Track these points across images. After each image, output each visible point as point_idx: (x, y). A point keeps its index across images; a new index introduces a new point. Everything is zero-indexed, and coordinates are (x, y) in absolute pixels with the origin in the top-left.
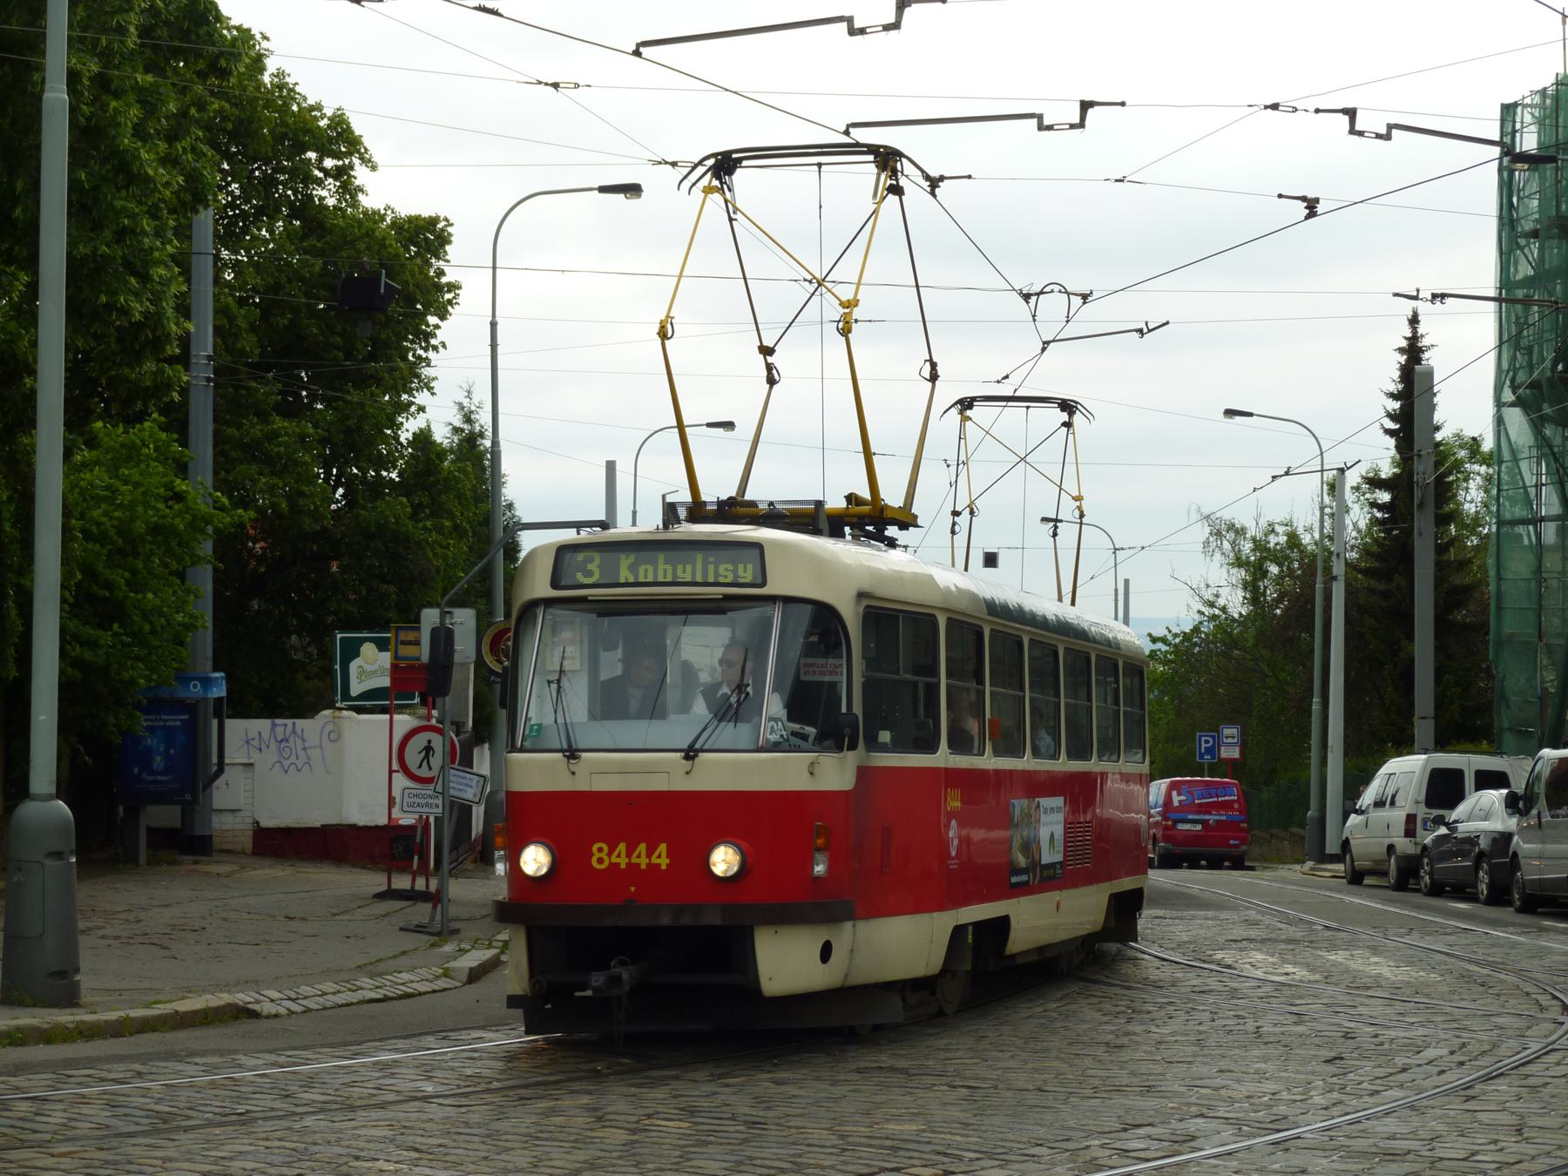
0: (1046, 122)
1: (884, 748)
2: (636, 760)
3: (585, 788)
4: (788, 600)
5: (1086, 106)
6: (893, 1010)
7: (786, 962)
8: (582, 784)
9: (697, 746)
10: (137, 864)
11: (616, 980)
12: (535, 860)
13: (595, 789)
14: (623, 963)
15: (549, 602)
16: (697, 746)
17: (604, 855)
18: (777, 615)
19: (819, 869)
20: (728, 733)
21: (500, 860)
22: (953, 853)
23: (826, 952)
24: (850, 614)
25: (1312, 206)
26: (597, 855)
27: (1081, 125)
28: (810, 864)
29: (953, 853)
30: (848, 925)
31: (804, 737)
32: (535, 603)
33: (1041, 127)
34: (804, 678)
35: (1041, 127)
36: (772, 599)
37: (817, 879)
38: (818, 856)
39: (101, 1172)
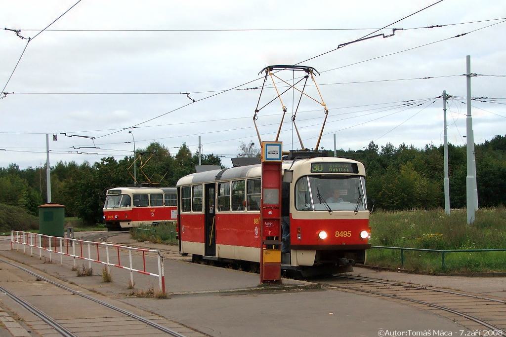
0: (382, 36)
5: (394, 30)
7: (123, 225)
15: (310, 176)
23: (129, 224)
27: (394, 35)
33: (384, 37)
35: (384, 37)
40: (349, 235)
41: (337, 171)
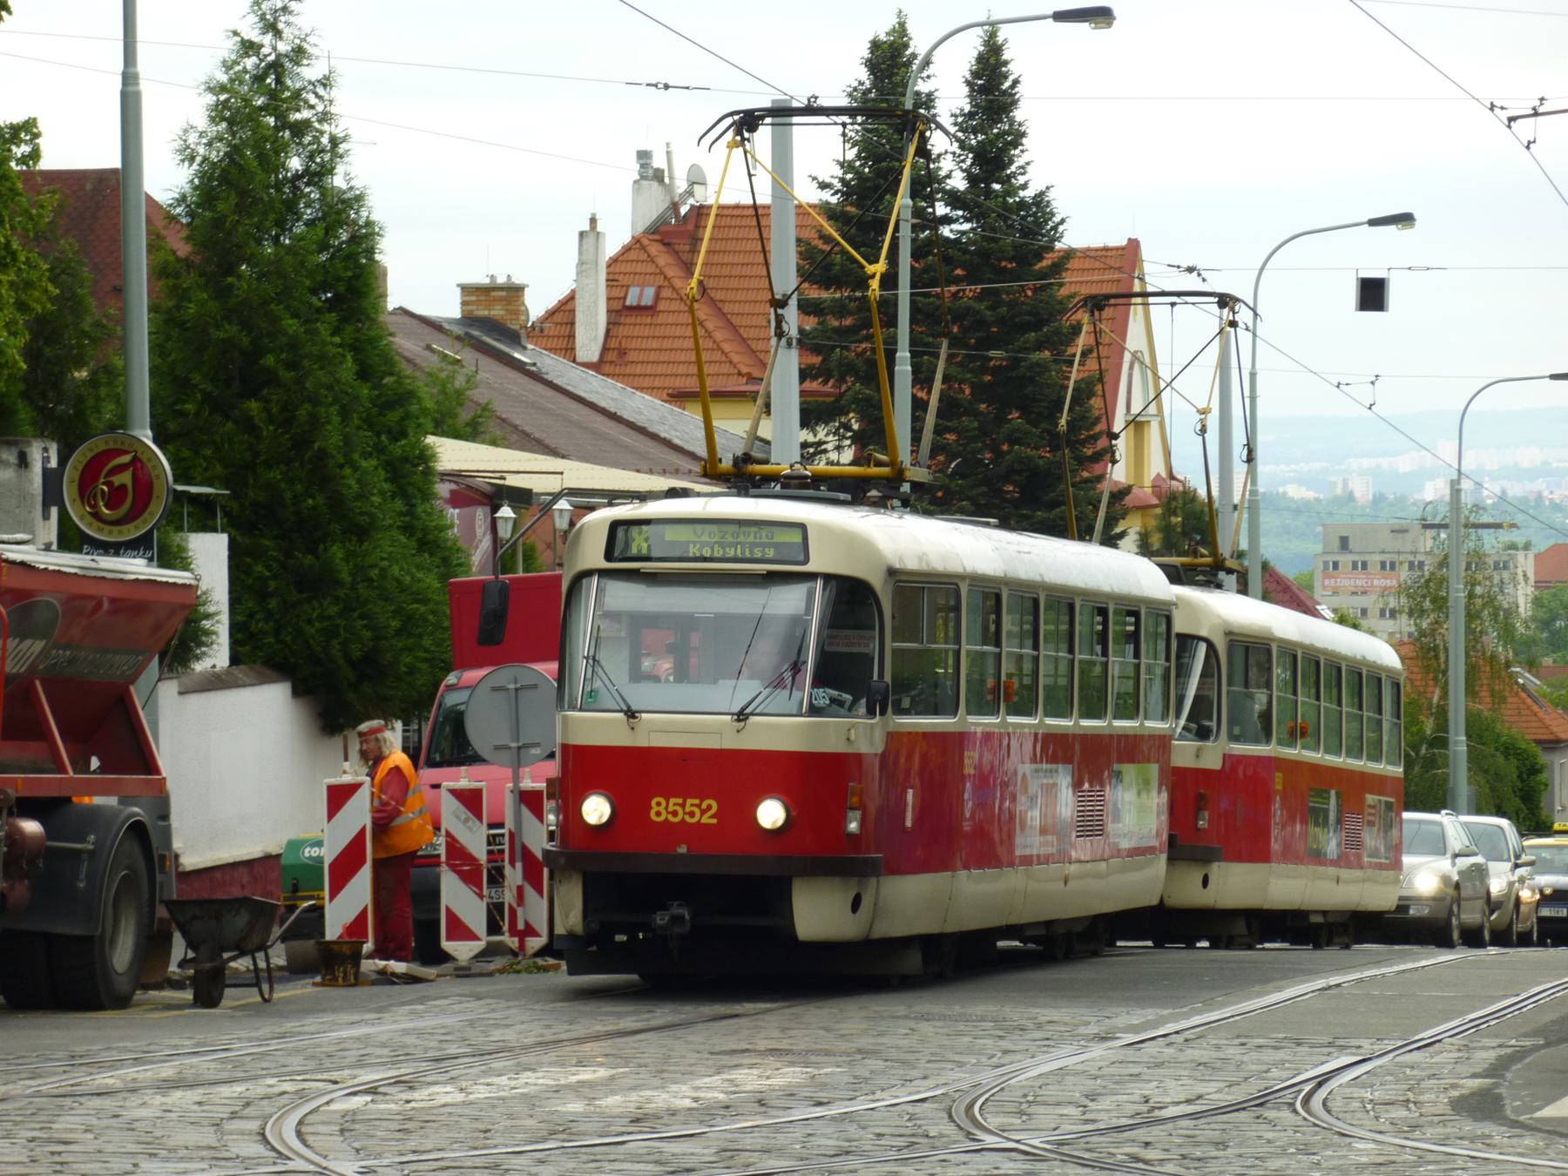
0: (587, 227)
1: (906, 712)
2: (692, 712)
3: (645, 744)
4: (828, 578)
6: (1240, 927)
7: (818, 913)
8: (642, 742)
9: (748, 711)
10: (89, 940)
11: (677, 919)
12: (596, 810)
13: (653, 744)
14: (680, 906)
15: (603, 573)
16: (748, 711)
17: (661, 809)
18: (819, 583)
19: (853, 826)
20: (781, 698)
21: (549, 811)
22: (967, 814)
23: (856, 905)
24: (877, 581)
25: (1492, 107)
26: (655, 809)
28: (843, 820)
29: (967, 814)
30: (873, 881)
31: (840, 703)
32: (588, 573)
33: (582, 234)
34: (827, 649)
36: (811, 576)
37: (852, 835)
38: (851, 814)
39: (1253, 1172)
40: (658, 814)
41: (731, 553)
